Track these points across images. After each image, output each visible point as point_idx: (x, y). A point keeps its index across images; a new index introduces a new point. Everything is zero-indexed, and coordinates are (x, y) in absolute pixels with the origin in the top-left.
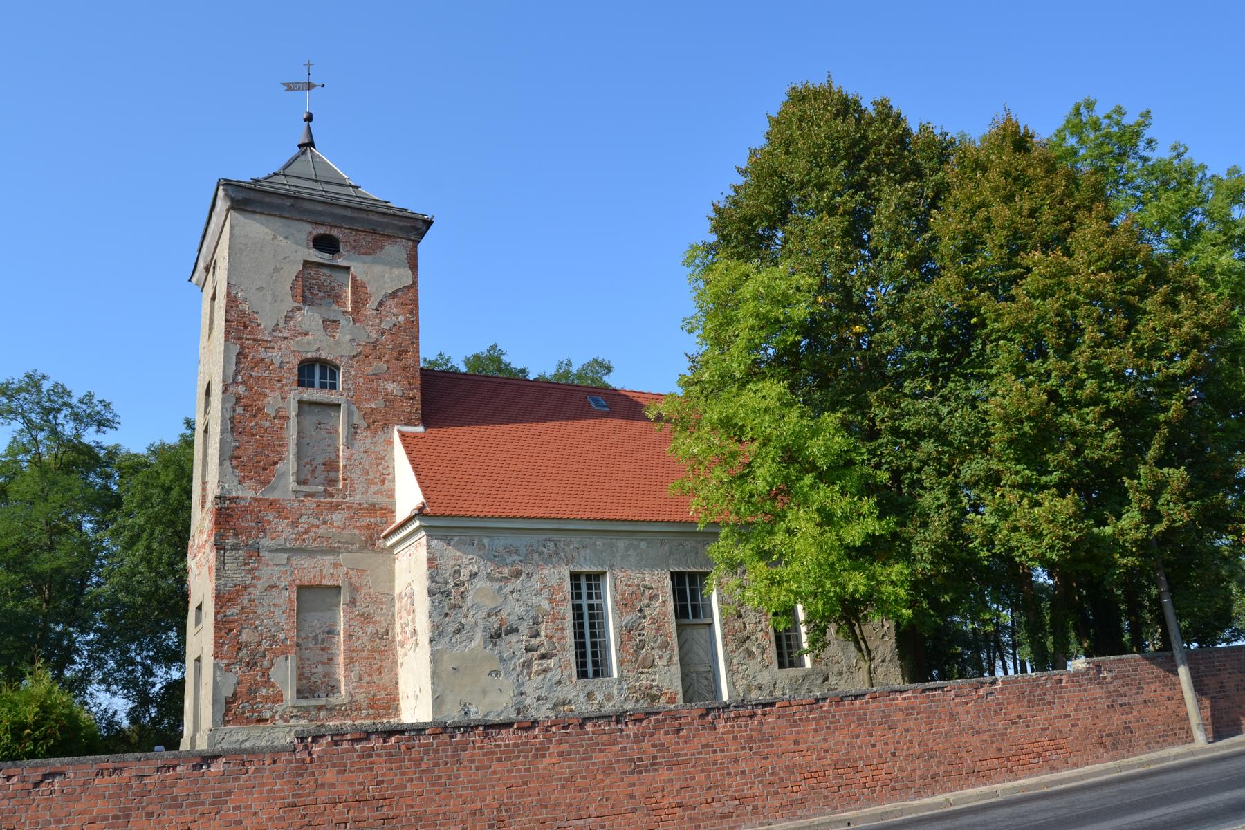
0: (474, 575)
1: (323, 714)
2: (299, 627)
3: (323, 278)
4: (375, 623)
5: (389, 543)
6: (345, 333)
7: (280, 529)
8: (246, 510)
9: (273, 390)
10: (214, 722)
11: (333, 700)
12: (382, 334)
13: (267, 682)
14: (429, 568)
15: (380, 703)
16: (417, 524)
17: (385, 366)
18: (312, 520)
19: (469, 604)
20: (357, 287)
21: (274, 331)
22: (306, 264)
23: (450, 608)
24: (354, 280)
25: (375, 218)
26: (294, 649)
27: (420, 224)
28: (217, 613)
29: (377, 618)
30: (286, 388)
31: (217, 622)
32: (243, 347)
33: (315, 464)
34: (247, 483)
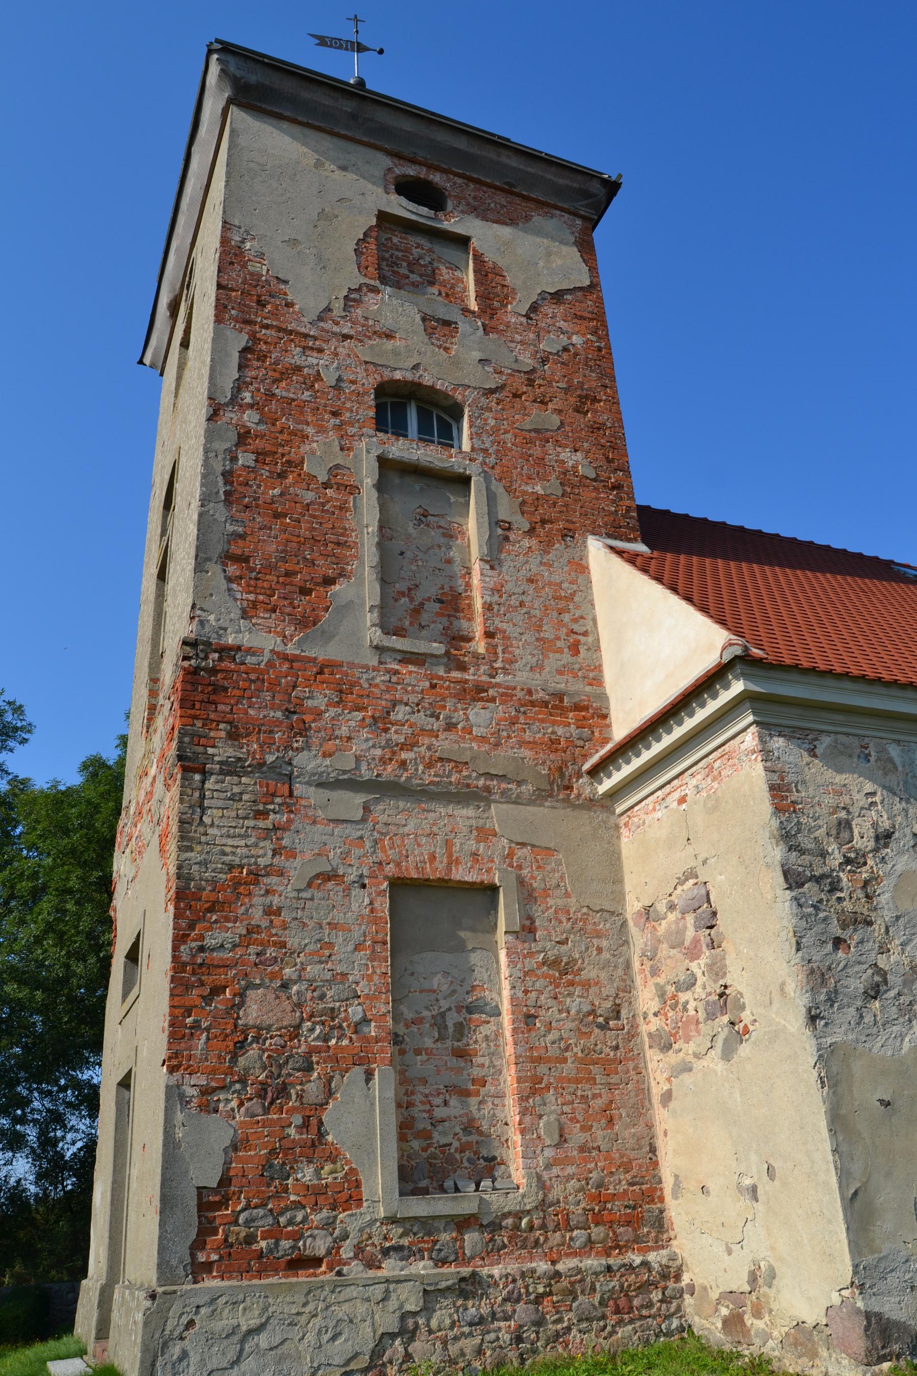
0: (884, 838)
1: (471, 1238)
2: (399, 988)
3: (416, 252)
4: (587, 985)
5: (606, 785)
6: (469, 345)
7: (344, 731)
8: (259, 678)
9: (322, 430)
10: (163, 1266)
11: (497, 1202)
12: (544, 361)
13: (316, 1145)
14: (778, 809)
15: (617, 1207)
16: (738, 687)
17: (556, 420)
18: (420, 719)
19: (888, 915)
20: (486, 274)
21: (320, 319)
22: (383, 217)
23: (844, 927)
24: (479, 259)
25: (514, 162)
26: (387, 1050)
27: (595, 187)
28: (179, 940)
29: (590, 973)
30: (351, 430)
31: (178, 965)
32: (253, 337)
33: (419, 596)
34: (263, 618)
